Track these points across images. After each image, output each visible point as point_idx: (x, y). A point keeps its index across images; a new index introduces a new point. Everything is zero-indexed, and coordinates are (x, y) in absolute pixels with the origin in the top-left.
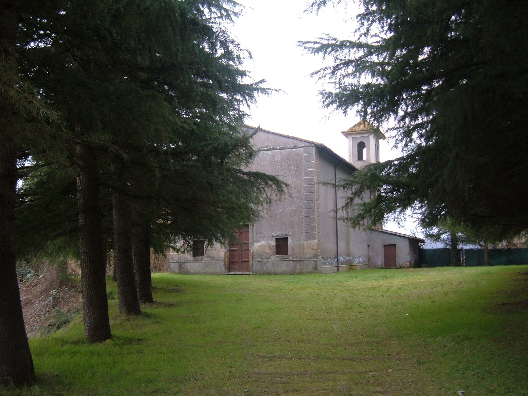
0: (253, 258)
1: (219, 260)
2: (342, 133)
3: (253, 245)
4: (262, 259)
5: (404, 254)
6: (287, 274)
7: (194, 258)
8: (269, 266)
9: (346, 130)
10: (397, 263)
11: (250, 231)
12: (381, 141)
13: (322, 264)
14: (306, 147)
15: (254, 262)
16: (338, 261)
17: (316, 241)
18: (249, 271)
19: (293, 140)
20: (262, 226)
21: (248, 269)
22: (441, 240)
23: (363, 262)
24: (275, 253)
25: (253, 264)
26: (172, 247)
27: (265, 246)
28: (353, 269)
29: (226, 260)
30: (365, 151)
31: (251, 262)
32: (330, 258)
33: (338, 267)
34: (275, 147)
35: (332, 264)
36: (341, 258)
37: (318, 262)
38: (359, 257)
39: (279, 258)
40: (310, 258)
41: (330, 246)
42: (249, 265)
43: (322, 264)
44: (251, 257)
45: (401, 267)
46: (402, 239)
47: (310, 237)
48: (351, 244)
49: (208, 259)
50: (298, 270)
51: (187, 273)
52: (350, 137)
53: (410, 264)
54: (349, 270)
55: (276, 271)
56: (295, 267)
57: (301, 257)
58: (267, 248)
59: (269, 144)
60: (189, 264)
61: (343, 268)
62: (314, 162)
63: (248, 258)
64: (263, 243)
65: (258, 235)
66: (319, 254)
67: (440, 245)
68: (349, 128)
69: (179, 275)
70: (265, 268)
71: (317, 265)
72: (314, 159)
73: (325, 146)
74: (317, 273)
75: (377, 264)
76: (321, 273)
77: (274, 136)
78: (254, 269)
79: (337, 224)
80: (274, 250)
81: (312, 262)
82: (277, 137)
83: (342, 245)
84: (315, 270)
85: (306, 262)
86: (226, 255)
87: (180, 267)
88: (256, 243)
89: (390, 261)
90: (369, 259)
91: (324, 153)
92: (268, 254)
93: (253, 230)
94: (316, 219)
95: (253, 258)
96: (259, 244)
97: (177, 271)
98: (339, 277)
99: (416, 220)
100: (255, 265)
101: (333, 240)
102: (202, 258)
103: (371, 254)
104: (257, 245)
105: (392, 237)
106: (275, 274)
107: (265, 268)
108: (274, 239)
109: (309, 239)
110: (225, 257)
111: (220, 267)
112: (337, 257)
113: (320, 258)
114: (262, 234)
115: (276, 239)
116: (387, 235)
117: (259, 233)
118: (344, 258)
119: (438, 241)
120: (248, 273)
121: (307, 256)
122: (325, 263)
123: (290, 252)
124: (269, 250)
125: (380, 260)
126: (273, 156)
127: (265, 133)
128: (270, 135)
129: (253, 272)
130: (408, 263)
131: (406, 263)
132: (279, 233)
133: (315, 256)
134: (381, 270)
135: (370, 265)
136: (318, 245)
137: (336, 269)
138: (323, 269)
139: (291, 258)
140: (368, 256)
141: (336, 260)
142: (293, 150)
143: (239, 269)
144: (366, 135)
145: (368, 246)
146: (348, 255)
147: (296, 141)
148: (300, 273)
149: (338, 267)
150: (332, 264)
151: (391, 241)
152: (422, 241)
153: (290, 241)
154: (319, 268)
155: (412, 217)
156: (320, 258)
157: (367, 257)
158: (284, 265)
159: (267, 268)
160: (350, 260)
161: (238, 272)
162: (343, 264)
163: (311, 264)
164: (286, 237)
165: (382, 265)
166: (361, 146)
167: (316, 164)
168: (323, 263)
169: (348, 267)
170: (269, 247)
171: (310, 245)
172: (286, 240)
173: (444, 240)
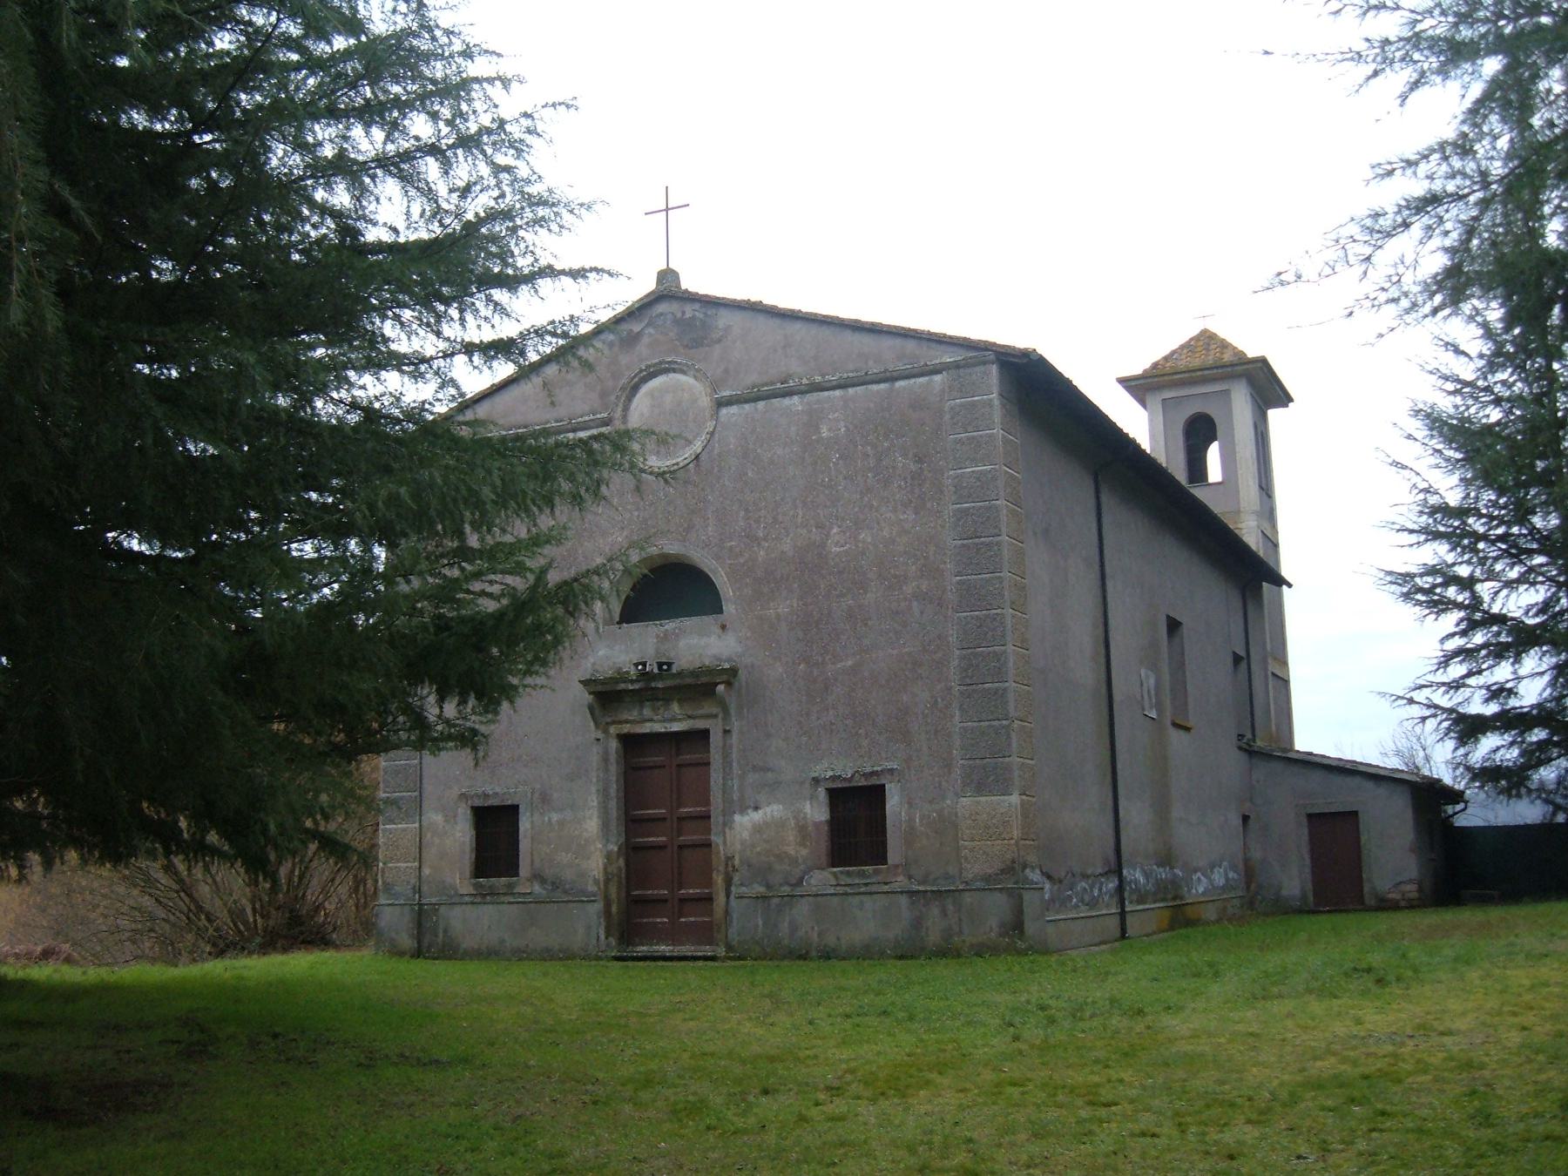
0: (728, 882)
1: (583, 892)
2: (1125, 382)
3: (727, 824)
4: (768, 887)
5: (1392, 853)
6: (882, 955)
7: (476, 886)
8: (801, 921)
9: (1137, 368)
10: (1366, 889)
11: (715, 756)
12: (1273, 414)
13: (1047, 906)
14: (957, 366)
15: (733, 902)
16: (1120, 889)
17: (1015, 799)
18: (711, 941)
19: (898, 342)
20: (769, 736)
21: (706, 933)
22: (1530, 791)
23: (1227, 887)
24: (824, 860)
25: (727, 912)
26: (314, 834)
27: (781, 824)
28: (1190, 923)
29: (613, 891)
30: (1213, 454)
31: (721, 899)
32: (1085, 876)
33: (1123, 914)
34: (818, 379)
35: (1093, 904)
36: (1134, 875)
37: (1027, 896)
38: (1212, 867)
39: (845, 880)
40: (987, 879)
41: (1082, 817)
42: (710, 913)
43: (1047, 906)
44: (719, 879)
45: (1385, 905)
46: (1382, 790)
47: (987, 780)
48: (1177, 812)
49: (537, 888)
50: (933, 937)
51: (449, 951)
52: (1155, 400)
53: (1420, 890)
54: (1171, 928)
55: (831, 940)
56: (917, 923)
57: (947, 877)
58: (791, 836)
59: (795, 367)
60: (457, 910)
61: (1144, 917)
62: (998, 432)
63: (709, 883)
64: (774, 810)
65: (752, 778)
66: (1032, 858)
67: (1528, 812)
68: (1147, 365)
69: (419, 967)
70: (785, 927)
71: (1019, 911)
72: (997, 415)
73: (1042, 358)
74: (1021, 953)
75: (1284, 892)
76: (1043, 949)
77: (814, 330)
78: (734, 934)
79: (1105, 598)
80: (823, 845)
81: (998, 894)
82: (826, 332)
83: (1136, 815)
84: (1015, 939)
85: (968, 898)
86: (613, 869)
87: (419, 925)
88: (743, 811)
89: (1338, 882)
90: (1249, 872)
91: (1034, 388)
92: (794, 861)
93: (726, 756)
94: (1011, 696)
95: (728, 882)
96: (757, 816)
97: (406, 941)
98: (1132, 975)
99: (1428, 713)
100: (740, 915)
101: (1095, 794)
102: (511, 886)
103: (1256, 854)
104: (744, 823)
105: (1338, 780)
106: (827, 955)
107: (785, 927)
108: (822, 793)
109: (980, 788)
110: (607, 881)
111: (586, 924)
112: (1117, 870)
113: (1035, 876)
114: (767, 769)
115: (834, 794)
116: (1317, 776)
117: (755, 769)
118: (1147, 875)
119: (1519, 796)
120: (707, 950)
121: (973, 869)
122: (1059, 902)
123: (894, 854)
124: (802, 844)
125: (1294, 880)
126: (813, 420)
127: (778, 321)
128: (798, 325)
129: (729, 947)
130: (1414, 887)
131: (1409, 887)
132: (845, 767)
133: (1012, 869)
134: (1307, 920)
135: (1255, 903)
136: (1025, 815)
137: (1114, 923)
138: (1050, 929)
139: (900, 882)
140: (1246, 861)
141: (1112, 885)
142: (899, 384)
143: (672, 934)
144: (1217, 387)
145: (1245, 819)
146: (1166, 860)
147: (910, 345)
148: (947, 951)
149: (1123, 914)
150: (1093, 904)
151: (1339, 797)
152: (1455, 796)
153: (893, 802)
154: (1030, 927)
155: (1411, 701)
156: (1035, 876)
157: (1241, 866)
158: (869, 914)
159: (794, 928)
160: (1175, 882)
161: (663, 948)
162: (1139, 902)
163: (996, 907)
164: (874, 781)
165: (1304, 897)
166: (1200, 432)
167: (1006, 441)
168: (1052, 900)
169: (1167, 913)
170: (802, 828)
171: (985, 822)
172: (874, 795)
173: (1542, 788)
